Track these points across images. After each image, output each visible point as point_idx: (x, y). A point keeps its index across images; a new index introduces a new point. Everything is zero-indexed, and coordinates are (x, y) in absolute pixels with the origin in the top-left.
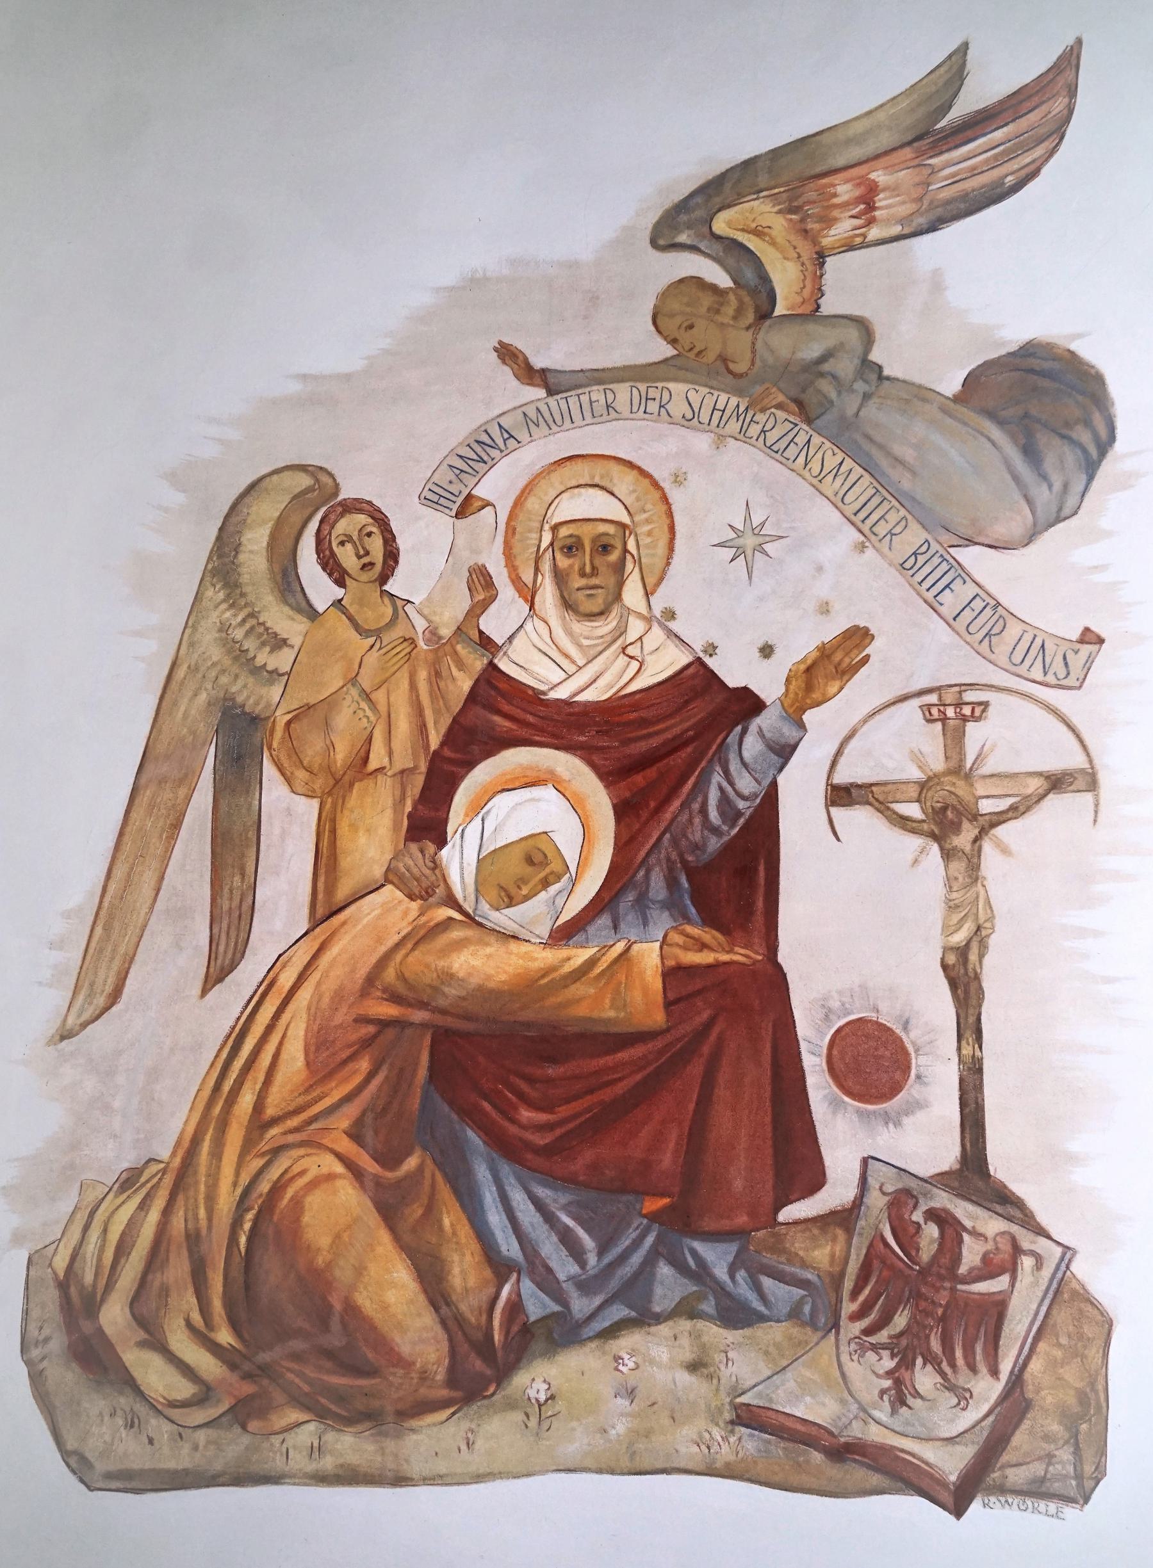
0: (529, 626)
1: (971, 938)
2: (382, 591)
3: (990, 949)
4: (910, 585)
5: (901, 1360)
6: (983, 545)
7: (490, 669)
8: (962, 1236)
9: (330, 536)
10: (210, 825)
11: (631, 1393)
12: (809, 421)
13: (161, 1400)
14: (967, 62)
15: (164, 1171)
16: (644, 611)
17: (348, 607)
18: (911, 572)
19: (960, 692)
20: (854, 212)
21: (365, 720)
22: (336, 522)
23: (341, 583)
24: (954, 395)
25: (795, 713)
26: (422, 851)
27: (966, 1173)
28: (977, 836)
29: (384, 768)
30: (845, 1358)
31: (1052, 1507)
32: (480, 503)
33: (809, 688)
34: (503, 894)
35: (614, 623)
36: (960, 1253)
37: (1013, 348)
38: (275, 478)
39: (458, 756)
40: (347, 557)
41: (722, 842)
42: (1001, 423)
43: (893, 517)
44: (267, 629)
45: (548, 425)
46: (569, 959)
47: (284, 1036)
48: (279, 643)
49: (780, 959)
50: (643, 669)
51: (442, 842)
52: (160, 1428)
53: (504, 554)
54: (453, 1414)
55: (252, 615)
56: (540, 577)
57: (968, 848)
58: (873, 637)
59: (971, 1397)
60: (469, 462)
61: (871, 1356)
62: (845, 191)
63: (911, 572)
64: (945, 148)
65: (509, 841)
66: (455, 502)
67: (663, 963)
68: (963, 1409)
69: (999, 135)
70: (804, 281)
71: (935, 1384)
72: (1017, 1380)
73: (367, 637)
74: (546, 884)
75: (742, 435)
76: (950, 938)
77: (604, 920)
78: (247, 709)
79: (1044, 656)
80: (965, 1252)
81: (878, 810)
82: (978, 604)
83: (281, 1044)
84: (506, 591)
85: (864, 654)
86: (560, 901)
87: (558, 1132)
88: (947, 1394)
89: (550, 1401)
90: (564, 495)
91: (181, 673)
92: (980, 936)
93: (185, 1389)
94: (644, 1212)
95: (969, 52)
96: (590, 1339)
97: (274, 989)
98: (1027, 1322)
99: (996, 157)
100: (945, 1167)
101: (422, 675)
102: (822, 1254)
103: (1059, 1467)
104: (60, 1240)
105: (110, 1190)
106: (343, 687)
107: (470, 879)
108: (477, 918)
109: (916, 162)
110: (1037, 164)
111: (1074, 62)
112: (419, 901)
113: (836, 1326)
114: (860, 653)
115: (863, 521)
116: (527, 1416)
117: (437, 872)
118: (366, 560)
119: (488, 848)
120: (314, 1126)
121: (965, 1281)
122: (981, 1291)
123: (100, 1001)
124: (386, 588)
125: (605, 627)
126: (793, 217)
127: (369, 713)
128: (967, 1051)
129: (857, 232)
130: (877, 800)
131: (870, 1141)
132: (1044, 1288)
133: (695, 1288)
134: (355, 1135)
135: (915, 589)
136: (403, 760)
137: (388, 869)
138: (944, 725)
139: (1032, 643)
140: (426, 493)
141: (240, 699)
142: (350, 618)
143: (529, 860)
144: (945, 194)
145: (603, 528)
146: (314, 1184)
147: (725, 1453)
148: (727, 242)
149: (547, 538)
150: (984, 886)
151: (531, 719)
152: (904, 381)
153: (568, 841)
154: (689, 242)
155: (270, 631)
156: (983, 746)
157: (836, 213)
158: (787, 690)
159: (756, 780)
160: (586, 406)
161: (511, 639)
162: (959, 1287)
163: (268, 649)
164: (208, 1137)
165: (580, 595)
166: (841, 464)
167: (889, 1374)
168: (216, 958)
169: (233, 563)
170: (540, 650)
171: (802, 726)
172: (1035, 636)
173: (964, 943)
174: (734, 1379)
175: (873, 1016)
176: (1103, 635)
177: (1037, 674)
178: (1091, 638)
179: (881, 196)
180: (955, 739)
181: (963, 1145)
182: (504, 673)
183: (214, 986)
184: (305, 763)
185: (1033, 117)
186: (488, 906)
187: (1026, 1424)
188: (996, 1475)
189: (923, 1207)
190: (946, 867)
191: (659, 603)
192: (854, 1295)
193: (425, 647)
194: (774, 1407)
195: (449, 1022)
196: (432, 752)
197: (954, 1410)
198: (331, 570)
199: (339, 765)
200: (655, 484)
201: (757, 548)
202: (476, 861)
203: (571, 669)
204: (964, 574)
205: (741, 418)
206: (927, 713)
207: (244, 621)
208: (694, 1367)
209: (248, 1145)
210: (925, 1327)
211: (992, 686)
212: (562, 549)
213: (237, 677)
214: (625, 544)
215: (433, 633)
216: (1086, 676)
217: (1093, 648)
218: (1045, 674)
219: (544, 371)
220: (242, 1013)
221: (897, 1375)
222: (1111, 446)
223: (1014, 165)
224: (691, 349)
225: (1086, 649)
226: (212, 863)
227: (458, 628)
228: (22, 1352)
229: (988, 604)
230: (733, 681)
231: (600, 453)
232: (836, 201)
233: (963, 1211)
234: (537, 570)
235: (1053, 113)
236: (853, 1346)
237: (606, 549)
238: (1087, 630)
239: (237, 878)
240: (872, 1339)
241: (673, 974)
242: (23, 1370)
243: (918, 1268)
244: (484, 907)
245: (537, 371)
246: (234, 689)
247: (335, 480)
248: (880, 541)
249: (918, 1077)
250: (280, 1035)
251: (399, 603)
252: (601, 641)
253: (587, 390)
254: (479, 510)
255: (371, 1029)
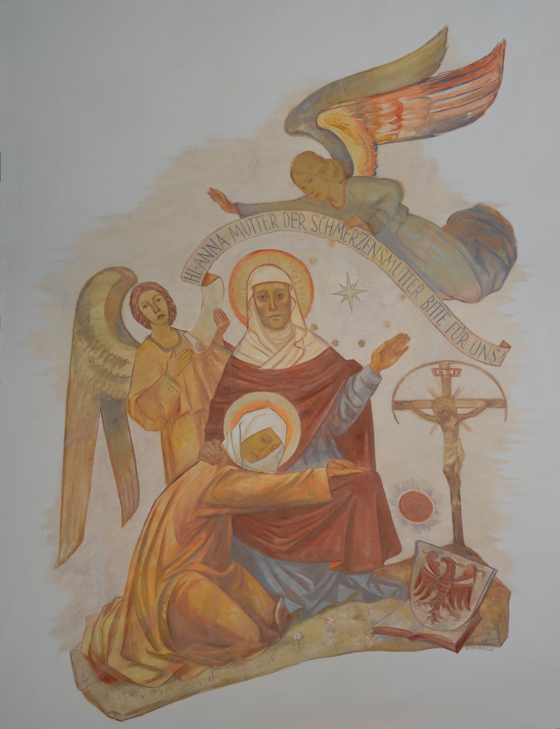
0: (248, 337)
1: (455, 462)
2: (171, 328)
3: (463, 466)
4: (426, 316)
5: (435, 607)
6: (458, 300)
7: (232, 358)
8: (455, 566)
9: (138, 303)
10: (108, 454)
11: (334, 630)
12: (374, 234)
13: (143, 682)
14: (448, 40)
15: (123, 600)
16: (302, 326)
17: (154, 338)
18: (426, 310)
19: (449, 364)
20: (391, 120)
21: (175, 391)
22: (139, 296)
23: (148, 327)
24: (443, 227)
25: (377, 369)
26: (214, 444)
27: (456, 545)
28: (456, 423)
29: (188, 412)
30: (413, 608)
31: (490, 648)
32: (214, 277)
33: (382, 360)
34: (254, 456)
35: (289, 332)
36: (455, 572)
37: (471, 206)
38: (100, 277)
39: (224, 400)
40: (149, 313)
41: (348, 425)
42: (465, 244)
43: (417, 284)
44: (115, 357)
45: (243, 234)
46: (287, 478)
47: (165, 533)
48: (123, 362)
49: (377, 470)
50: (305, 352)
51: (222, 438)
52: (145, 692)
53: (230, 302)
54: (265, 651)
55: (105, 351)
56: (250, 312)
57: (453, 427)
58: (409, 339)
59: (461, 617)
60: (204, 256)
61: (423, 607)
62: (386, 107)
63: (426, 310)
64: (437, 89)
65: (253, 434)
66: (200, 278)
67: (328, 476)
68: (458, 621)
69: (464, 87)
70: (367, 158)
71: (448, 614)
72: (477, 611)
73: (168, 352)
74: (272, 449)
75: (342, 240)
76: (446, 462)
77: (300, 461)
78: (114, 397)
79: (485, 351)
80: (456, 571)
81: (415, 412)
82: (456, 327)
83: (164, 536)
84: (234, 321)
85: (406, 346)
86: (280, 456)
87: (292, 544)
88: (452, 616)
89: (302, 639)
90: (256, 270)
91: (74, 387)
92: (459, 461)
93: (151, 675)
94: (331, 568)
95: (449, 33)
96: (315, 615)
97: (156, 515)
98: (480, 593)
99: (463, 100)
100: (448, 543)
101: (199, 366)
102: (402, 575)
103: (492, 636)
104: (82, 642)
105: (100, 615)
106: (161, 378)
107: (238, 451)
108: (244, 468)
109: (422, 95)
110: (484, 108)
111: (502, 54)
112: (216, 465)
113: (409, 598)
114: (404, 345)
115: (403, 285)
116: (294, 645)
117: (222, 451)
118: (159, 313)
119: (244, 438)
120: (186, 564)
121: (457, 581)
122: (463, 584)
123: (74, 543)
124: (173, 326)
125: (285, 334)
126: (360, 120)
127: (176, 388)
128: (455, 502)
129: (394, 132)
130: (414, 407)
131: (418, 535)
132: (486, 582)
133: (354, 592)
134: (205, 563)
135: (428, 318)
136: (197, 406)
137: (199, 455)
138: (442, 378)
139: (480, 345)
140: (184, 275)
141: (109, 393)
142: (158, 344)
143: (264, 441)
144: (437, 117)
145: (277, 286)
146: (190, 586)
147: (371, 643)
148: (326, 132)
149: (250, 293)
150: (460, 442)
151: (255, 379)
152: (419, 217)
153: (280, 430)
154: (306, 131)
155: (117, 357)
156: (459, 387)
157: (382, 120)
158: (372, 361)
159: (361, 399)
160: (261, 223)
161: (240, 343)
162: (455, 583)
163: (118, 366)
164: (139, 582)
165: (271, 320)
166: (391, 257)
167: (430, 612)
168: (125, 509)
169: (88, 326)
170: (255, 348)
171: (380, 377)
172: (481, 342)
173: (452, 464)
174: (372, 619)
175: (417, 491)
176: (511, 344)
177: (482, 358)
178: (505, 345)
179: (405, 112)
180: (446, 383)
181: (454, 536)
182: (239, 360)
183: (127, 521)
184: (150, 415)
185: (482, 81)
186: (248, 462)
187: (480, 624)
188: (470, 639)
189: (440, 557)
190: (444, 435)
191: (309, 322)
192: (416, 587)
193: (198, 352)
194: (388, 626)
195: (238, 511)
196: (210, 400)
197: (455, 622)
198: (142, 322)
199: (166, 414)
200: (301, 263)
201: (354, 296)
202: (239, 444)
203: (271, 355)
204: (450, 313)
205: (341, 231)
206: (434, 372)
207: (101, 355)
208: (356, 618)
209: (158, 578)
210: (443, 596)
211: (463, 363)
212: (258, 297)
213: (104, 382)
214: (289, 293)
215: (201, 345)
216: (503, 361)
217: (506, 350)
218: (485, 359)
219: (236, 204)
220: (143, 528)
221: (433, 612)
222: (515, 261)
223: (472, 106)
224: (312, 193)
225: (503, 350)
226: (114, 470)
227: (213, 341)
228: (78, 687)
229: (461, 327)
230: (347, 357)
231: (272, 249)
232: (382, 112)
233: (455, 558)
234: (248, 309)
235: (492, 81)
236: (416, 604)
237: (280, 296)
238: (503, 342)
239: (128, 475)
240: (423, 601)
241: (333, 479)
242: (81, 693)
243: (439, 577)
244: (246, 462)
245: (233, 204)
246: (104, 389)
247: (134, 274)
248: (411, 295)
249: (436, 512)
250: (163, 532)
251: (181, 333)
252: (283, 341)
253: (260, 215)
254: (214, 281)
255: (204, 520)
